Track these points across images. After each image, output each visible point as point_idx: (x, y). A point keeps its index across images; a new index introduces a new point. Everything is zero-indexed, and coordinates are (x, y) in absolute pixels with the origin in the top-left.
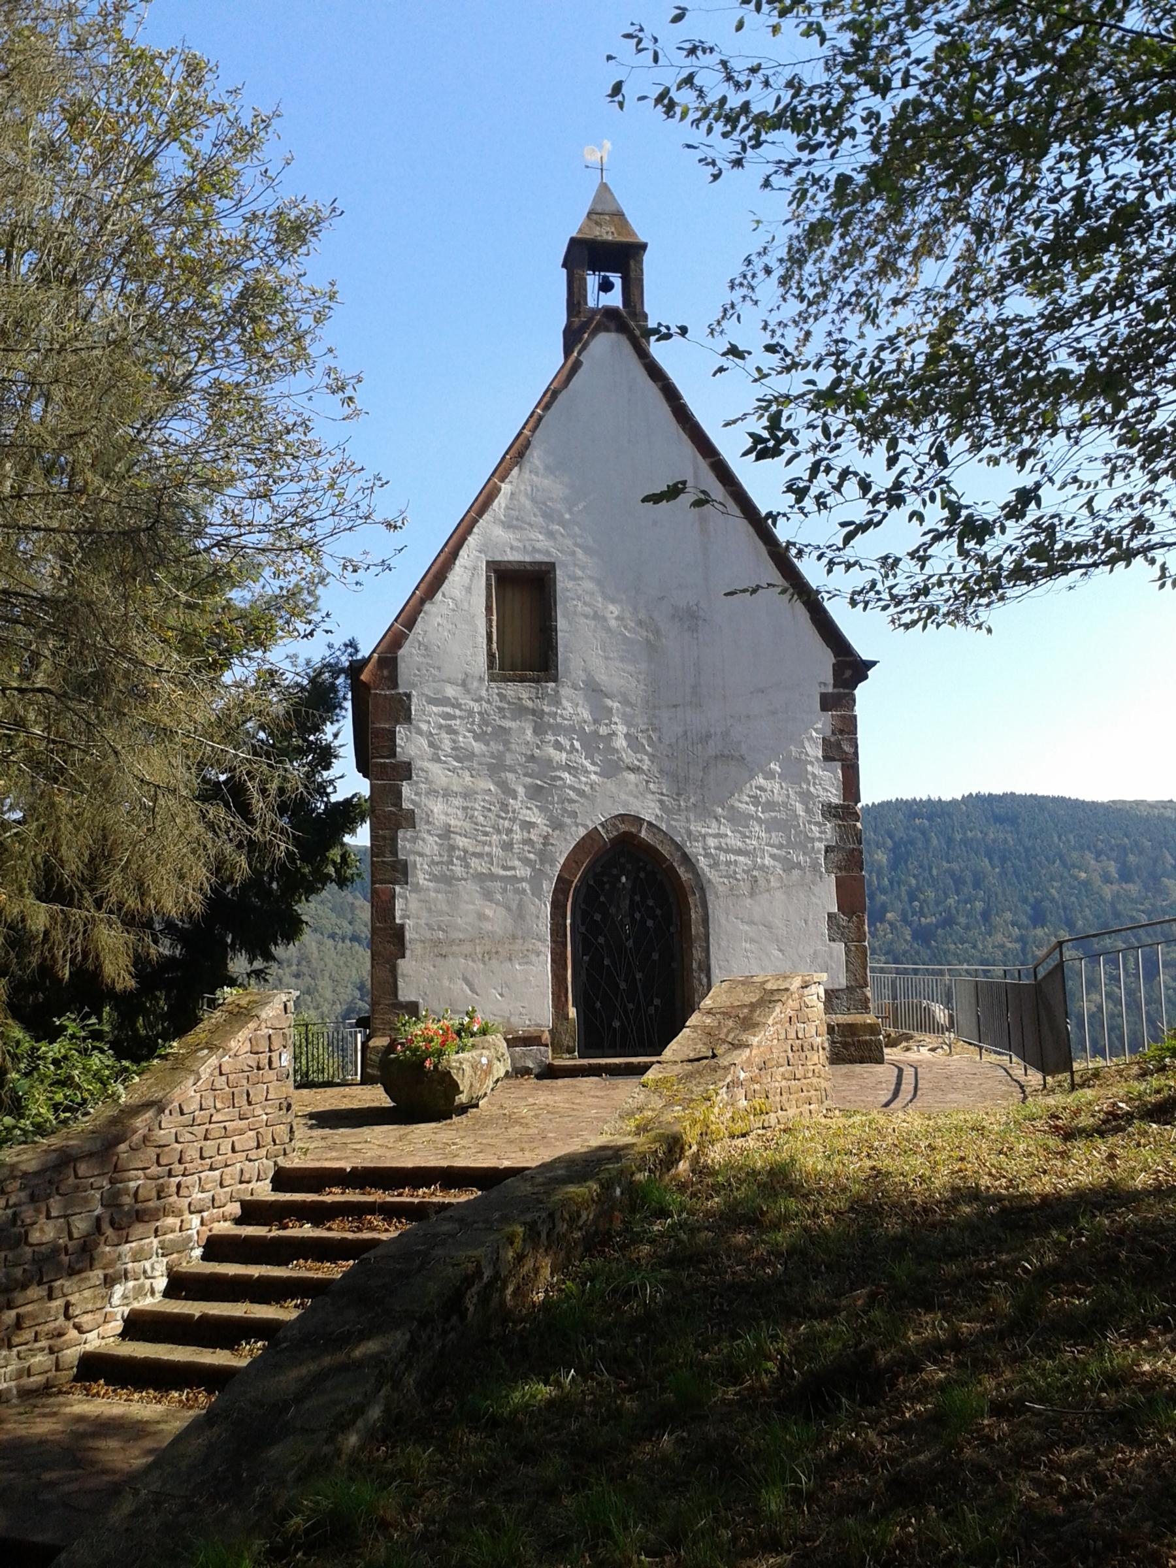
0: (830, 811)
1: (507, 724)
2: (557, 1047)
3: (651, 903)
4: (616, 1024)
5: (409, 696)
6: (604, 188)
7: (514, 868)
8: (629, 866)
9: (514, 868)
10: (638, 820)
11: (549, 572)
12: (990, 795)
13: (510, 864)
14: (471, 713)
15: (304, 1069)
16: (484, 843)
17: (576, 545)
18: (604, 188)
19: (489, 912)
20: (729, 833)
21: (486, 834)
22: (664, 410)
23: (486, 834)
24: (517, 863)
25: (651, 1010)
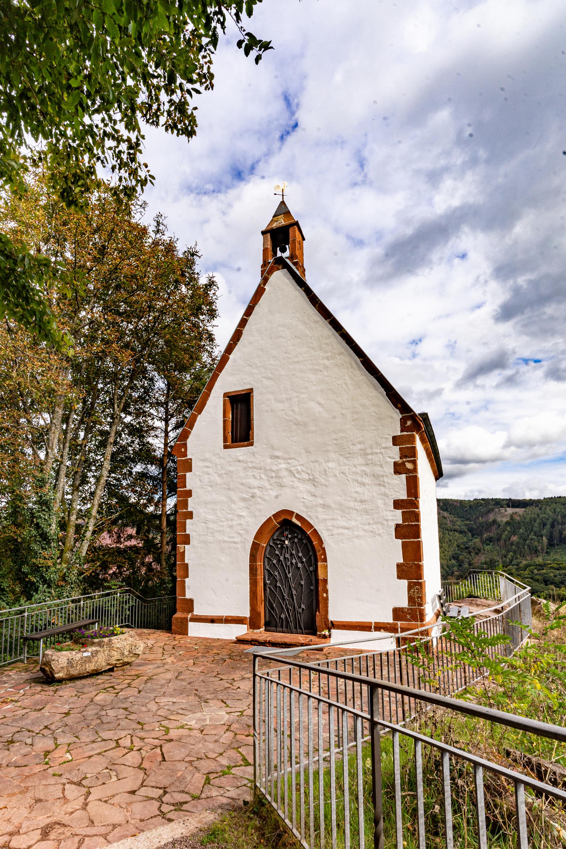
0: (398, 504)
1: (231, 469)
2: (253, 624)
3: (300, 555)
4: (283, 616)
5: (191, 459)
6: (283, 203)
7: (233, 537)
8: (290, 536)
9: (233, 537)
10: (291, 513)
11: (250, 393)
12: (531, 500)
13: (232, 535)
14: (216, 465)
15: (172, 717)
16: (221, 526)
17: (263, 377)
18: (283, 203)
19: (223, 559)
20: (339, 518)
21: (222, 521)
22: (251, 319)
23: (222, 521)
24: (235, 535)
25: (300, 610)
